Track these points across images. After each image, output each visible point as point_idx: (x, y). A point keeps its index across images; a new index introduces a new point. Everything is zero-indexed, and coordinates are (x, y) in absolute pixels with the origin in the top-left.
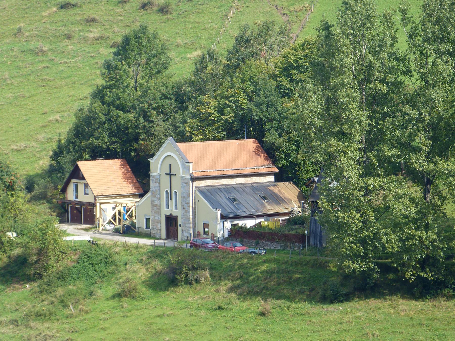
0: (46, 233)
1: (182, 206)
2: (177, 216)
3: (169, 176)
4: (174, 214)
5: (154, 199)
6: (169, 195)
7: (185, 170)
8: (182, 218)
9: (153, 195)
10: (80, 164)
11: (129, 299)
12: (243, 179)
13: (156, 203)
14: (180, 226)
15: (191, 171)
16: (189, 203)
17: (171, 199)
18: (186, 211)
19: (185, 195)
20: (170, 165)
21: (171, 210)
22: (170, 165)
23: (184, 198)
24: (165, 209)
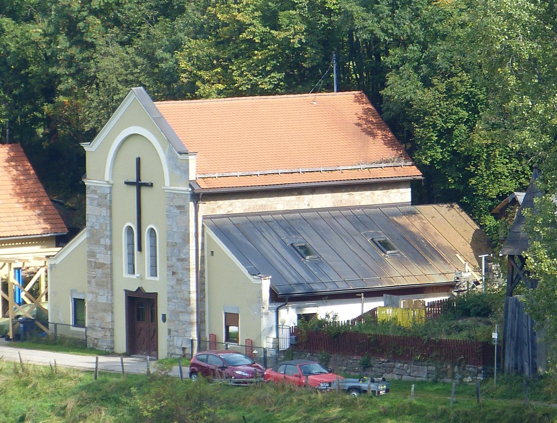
1: (170, 267)
2: (156, 294)
3: (134, 189)
5: (96, 248)
8: (169, 300)
9: (94, 239)
17: (140, 249)
18: (179, 281)
19: (177, 239)
20: (138, 160)
21: (141, 278)
22: (138, 160)
23: (174, 245)
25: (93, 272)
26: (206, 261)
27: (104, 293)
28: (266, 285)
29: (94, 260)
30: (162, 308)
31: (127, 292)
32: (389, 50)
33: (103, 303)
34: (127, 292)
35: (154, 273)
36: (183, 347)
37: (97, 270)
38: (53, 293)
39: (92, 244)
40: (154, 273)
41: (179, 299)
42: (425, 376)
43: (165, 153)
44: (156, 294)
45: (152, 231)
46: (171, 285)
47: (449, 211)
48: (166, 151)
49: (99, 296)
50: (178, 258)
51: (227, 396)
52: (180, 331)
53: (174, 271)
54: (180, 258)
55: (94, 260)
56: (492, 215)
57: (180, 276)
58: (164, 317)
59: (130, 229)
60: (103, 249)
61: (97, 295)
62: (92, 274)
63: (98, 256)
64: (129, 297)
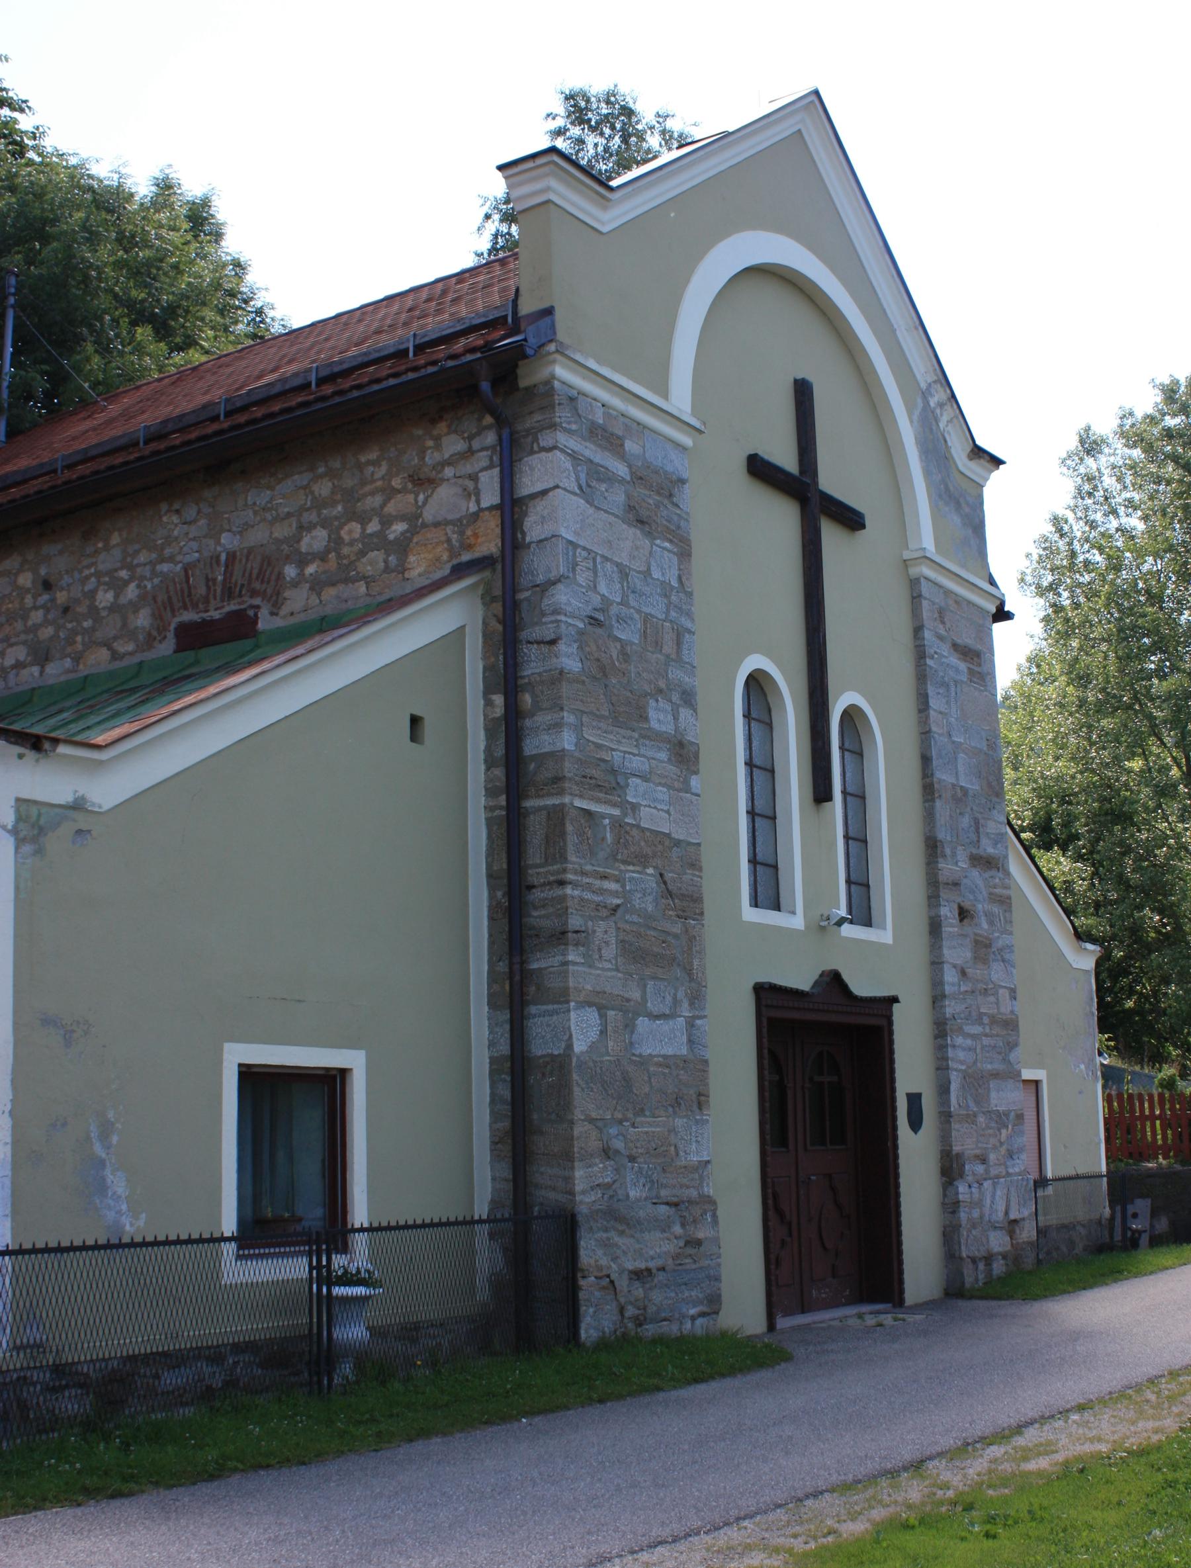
25: (605, 877)
27: (676, 1002)
29: (616, 812)
30: (1097, 1030)
31: (765, 993)
33: (667, 1062)
34: (765, 993)
36: (1012, 1217)
37: (632, 872)
38: (48, 1021)
39: (600, 718)
40: (862, 914)
41: (986, 1020)
43: (911, 422)
44: (240, 1065)
45: (851, 716)
46: (959, 962)
47: (495, 616)
48: (915, 417)
49: (642, 1023)
50: (974, 851)
51: (992, 1454)
52: (992, 1157)
53: (967, 905)
54: (981, 852)
55: (616, 812)
57: (985, 926)
58: (914, 1100)
59: (757, 684)
60: (663, 756)
61: (631, 1012)
62: (601, 892)
63: (635, 791)
64: (771, 1020)
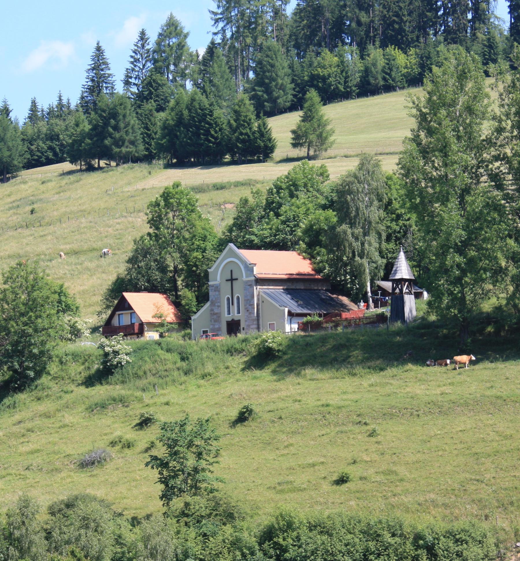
0: (504, 155)
1: (246, 309)
2: (239, 321)
3: (230, 283)
4: (236, 319)
5: (214, 308)
6: (230, 302)
7: (249, 272)
8: (246, 321)
9: (213, 304)
10: (127, 295)
11: (173, 420)
12: (225, 180)
13: (216, 311)
14: (243, 329)
15: (255, 273)
16: (254, 305)
17: (233, 304)
18: (250, 313)
19: (249, 298)
20: (231, 271)
21: (234, 315)
22: (231, 271)
23: (248, 300)
24: (226, 315)
26: (260, 307)
28: (286, 310)
32: (320, 237)
35: (239, 312)
42: (511, 178)
56: (513, 82)
59: (228, 299)
61: (214, 325)
